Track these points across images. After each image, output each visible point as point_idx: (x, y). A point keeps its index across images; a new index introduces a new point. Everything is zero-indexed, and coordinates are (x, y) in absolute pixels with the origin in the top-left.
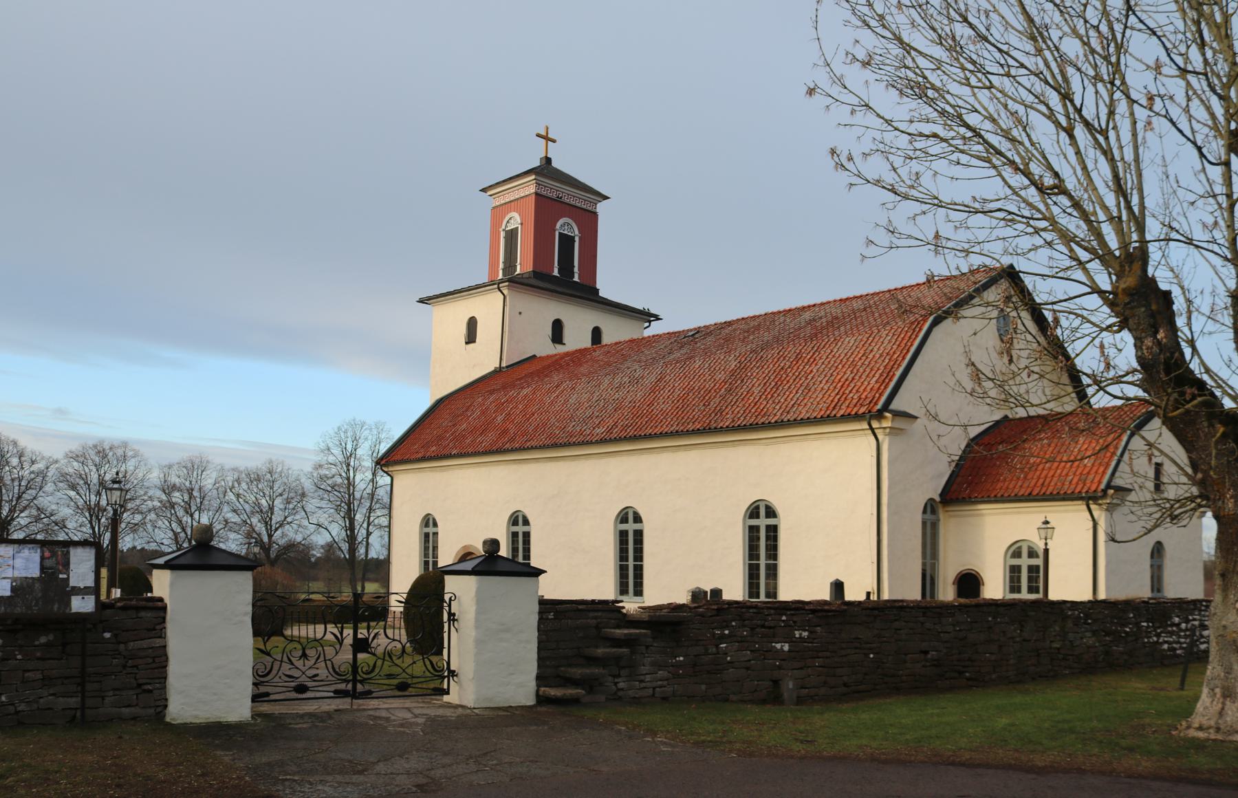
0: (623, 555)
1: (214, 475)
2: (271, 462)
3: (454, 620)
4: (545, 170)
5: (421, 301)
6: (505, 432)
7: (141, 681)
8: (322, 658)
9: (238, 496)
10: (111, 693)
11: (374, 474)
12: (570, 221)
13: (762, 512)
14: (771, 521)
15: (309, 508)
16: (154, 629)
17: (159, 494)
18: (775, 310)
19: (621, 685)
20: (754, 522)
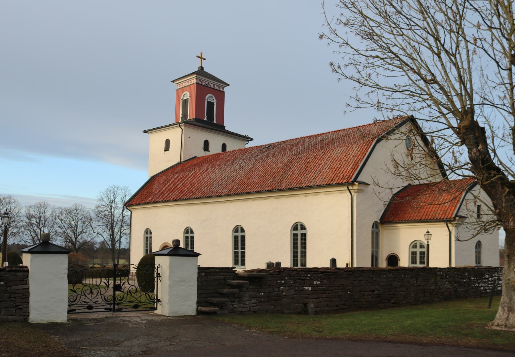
1: (50, 211)
2: (76, 205)
3: (159, 276)
4: (201, 72)
5: (144, 132)
6: (182, 191)
7: (17, 304)
8: (99, 294)
9: (61, 220)
10: (4, 309)
11: (123, 210)
12: (212, 95)
14: (303, 232)
17: (26, 219)
18: (305, 136)
19: (235, 306)
20: (295, 232)
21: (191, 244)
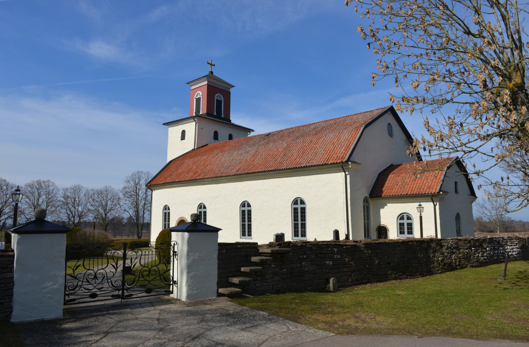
0: (243, 220)
1: (84, 192)
2: (106, 187)
3: (176, 255)
4: (210, 76)
5: (164, 124)
6: (197, 172)
8: (106, 278)
9: (93, 200)
11: (146, 191)
13: (299, 202)
14: (303, 206)
15: (121, 203)
16: (7, 267)
17: (62, 199)
18: (299, 125)
19: (258, 285)
20: (296, 206)
21: (302, 216)
